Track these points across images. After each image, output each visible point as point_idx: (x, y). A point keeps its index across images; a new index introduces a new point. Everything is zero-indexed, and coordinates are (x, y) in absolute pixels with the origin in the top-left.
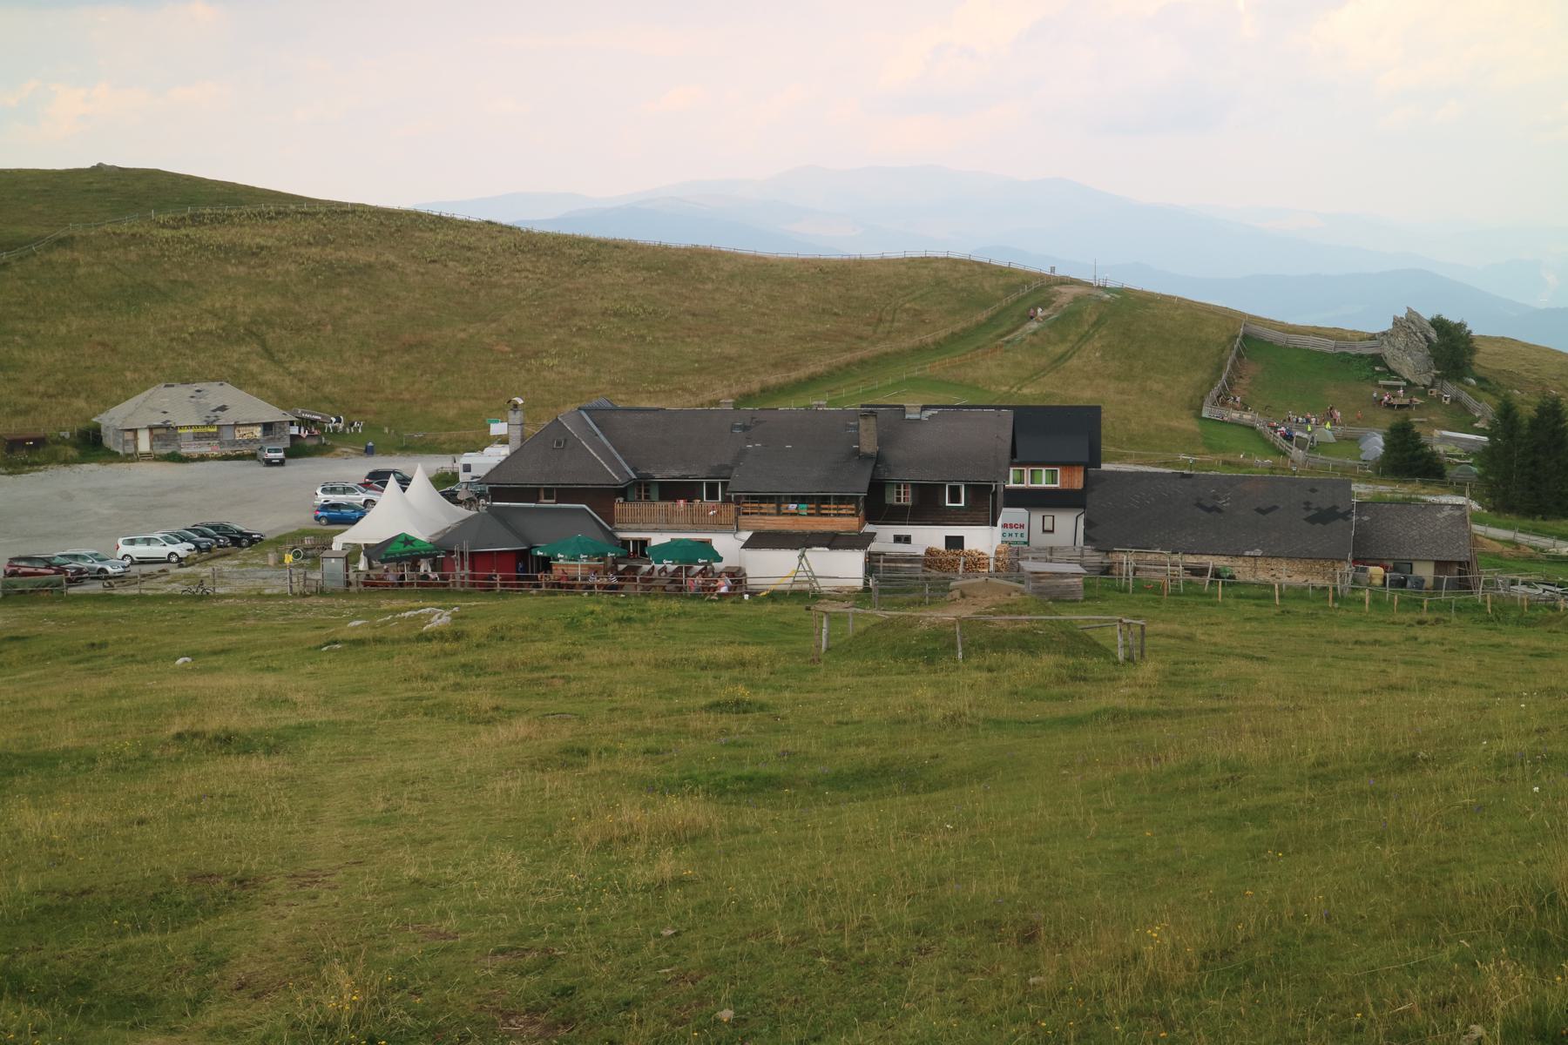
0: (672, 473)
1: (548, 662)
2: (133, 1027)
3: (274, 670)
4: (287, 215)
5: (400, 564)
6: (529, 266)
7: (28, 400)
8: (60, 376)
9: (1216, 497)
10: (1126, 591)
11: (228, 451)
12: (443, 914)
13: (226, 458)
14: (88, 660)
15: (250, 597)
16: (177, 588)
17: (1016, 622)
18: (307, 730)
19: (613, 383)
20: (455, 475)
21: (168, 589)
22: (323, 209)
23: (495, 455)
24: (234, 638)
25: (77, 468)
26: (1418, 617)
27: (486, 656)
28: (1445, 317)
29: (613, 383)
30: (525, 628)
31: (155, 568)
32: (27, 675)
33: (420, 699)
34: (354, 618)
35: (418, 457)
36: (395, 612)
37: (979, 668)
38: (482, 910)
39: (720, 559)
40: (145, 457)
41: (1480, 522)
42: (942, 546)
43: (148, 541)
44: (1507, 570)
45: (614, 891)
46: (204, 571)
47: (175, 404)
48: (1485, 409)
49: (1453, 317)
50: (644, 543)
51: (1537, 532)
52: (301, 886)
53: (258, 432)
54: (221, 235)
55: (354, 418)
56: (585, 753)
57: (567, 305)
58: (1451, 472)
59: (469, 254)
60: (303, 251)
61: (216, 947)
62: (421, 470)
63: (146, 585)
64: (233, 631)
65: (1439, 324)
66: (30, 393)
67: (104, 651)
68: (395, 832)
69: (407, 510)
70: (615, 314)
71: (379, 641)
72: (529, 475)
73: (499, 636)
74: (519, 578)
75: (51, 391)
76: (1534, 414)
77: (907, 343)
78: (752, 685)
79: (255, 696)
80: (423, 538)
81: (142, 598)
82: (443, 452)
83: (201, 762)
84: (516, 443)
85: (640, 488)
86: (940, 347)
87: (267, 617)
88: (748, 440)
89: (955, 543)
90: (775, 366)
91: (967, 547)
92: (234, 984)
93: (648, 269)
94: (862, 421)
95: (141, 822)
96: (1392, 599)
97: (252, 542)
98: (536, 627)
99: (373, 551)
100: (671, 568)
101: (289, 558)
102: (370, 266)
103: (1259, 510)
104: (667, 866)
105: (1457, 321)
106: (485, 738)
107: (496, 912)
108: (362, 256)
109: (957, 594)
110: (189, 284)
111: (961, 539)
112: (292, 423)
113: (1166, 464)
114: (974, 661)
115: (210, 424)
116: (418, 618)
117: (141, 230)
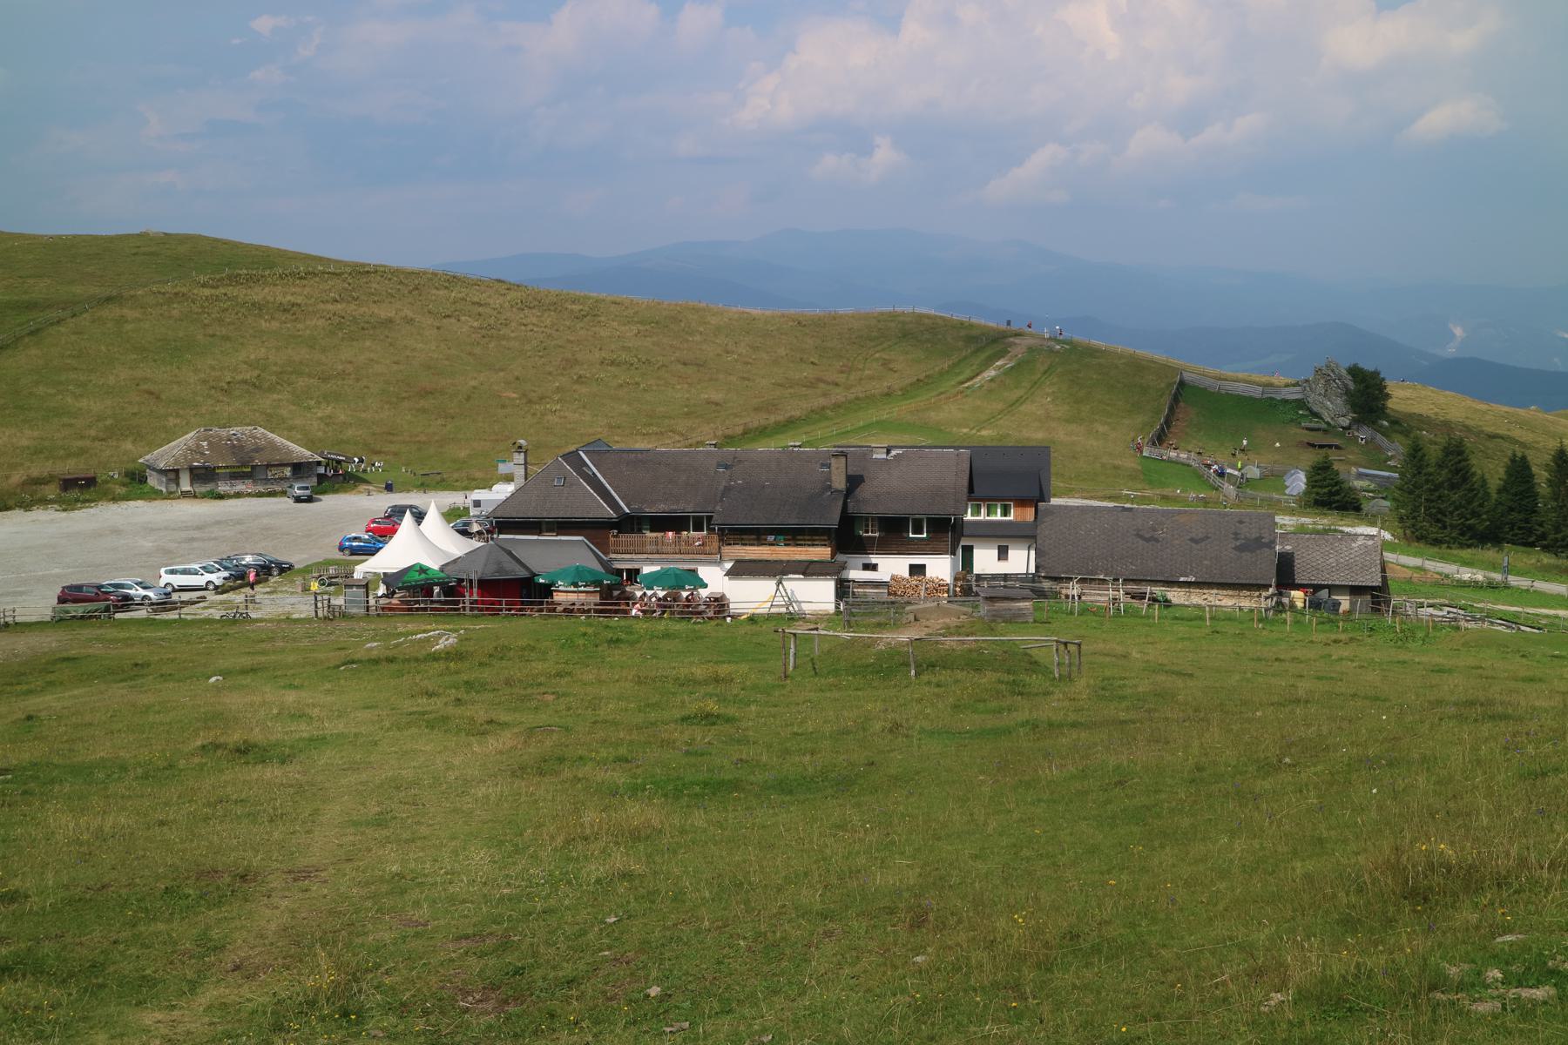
0: (660, 508)
1: (542, 679)
2: (139, 1004)
3: (296, 687)
4: (315, 275)
5: (420, 592)
6: (534, 320)
7: (80, 443)
8: (108, 422)
9: (1155, 530)
10: (1072, 613)
12: (417, 904)
13: (260, 495)
14: (131, 679)
15: (279, 621)
16: (216, 614)
17: (963, 642)
18: (318, 741)
19: (610, 427)
20: (467, 509)
21: (205, 614)
22: (348, 270)
23: (502, 491)
24: (263, 659)
25: (124, 505)
26: (1334, 637)
27: (486, 675)
28: (1361, 365)
29: (610, 427)
30: (523, 649)
31: (194, 595)
32: (76, 692)
33: (424, 713)
34: (373, 639)
35: (432, 493)
36: (407, 634)
37: (929, 683)
38: (452, 900)
39: (706, 586)
40: (185, 495)
41: (1393, 550)
42: (906, 574)
43: (185, 572)
44: (1416, 593)
45: (569, 883)
46: (237, 597)
48: (1396, 449)
49: (1368, 366)
50: (637, 571)
51: (1443, 559)
52: (295, 880)
53: (288, 472)
54: (258, 294)
55: (375, 458)
56: (561, 760)
57: (569, 355)
58: (1366, 507)
59: (481, 309)
60: (330, 307)
61: (215, 933)
62: (434, 504)
63: (185, 610)
64: (264, 653)
65: (1355, 372)
66: (82, 437)
67: (145, 671)
68: (385, 832)
69: (426, 543)
70: (613, 363)
71: (391, 660)
72: (530, 512)
73: (501, 653)
74: (522, 603)
75: (101, 435)
76: (1440, 454)
77: (877, 387)
78: (722, 699)
79: (275, 711)
80: (436, 567)
81: (181, 622)
82: (454, 489)
83: (221, 771)
84: (520, 481)
85: (629, 524)
87: (294, 640)
89: (917, 570)
90: (757, 409)
91: (929, 574)
92: (230, 966)
93: (641, 323)
94: (833, 461)
95: (162, 823)
96: (1310, 621)
97: (282, 571)
98: (533, 649)
99: (388, 579)
100: (661, 594)
101: (315, 586)
102: (391, 321)
103: (1192, 540)
104: (619, 860)
105: (1371, 369)
106: (476, 748)
107: (464, 901)
108: (384, 312)
109: (911, 617)
110: (227, 338)
111: (923, 566)
112: (319, 463)
113: (1110, 498)
114: (925, 678)
115: (244, 465)
116: (427, 640)
117: (184, 290)
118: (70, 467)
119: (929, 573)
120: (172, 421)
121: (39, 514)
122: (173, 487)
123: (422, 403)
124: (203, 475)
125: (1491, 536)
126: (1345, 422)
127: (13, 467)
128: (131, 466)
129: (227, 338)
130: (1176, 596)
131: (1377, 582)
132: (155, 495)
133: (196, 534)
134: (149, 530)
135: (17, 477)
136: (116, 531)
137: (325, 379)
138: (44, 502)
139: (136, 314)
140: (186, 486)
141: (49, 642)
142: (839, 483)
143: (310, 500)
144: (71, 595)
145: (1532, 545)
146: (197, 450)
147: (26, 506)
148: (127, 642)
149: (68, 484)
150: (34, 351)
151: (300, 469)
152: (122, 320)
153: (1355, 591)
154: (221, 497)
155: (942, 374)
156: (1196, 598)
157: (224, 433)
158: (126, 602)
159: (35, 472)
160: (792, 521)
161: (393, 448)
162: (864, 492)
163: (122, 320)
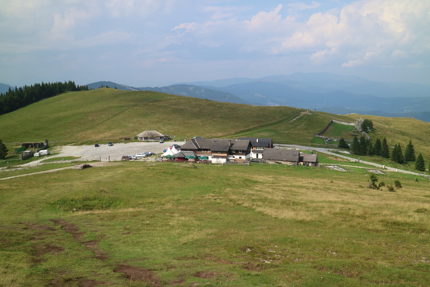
0: (205, 148)
5: (171, 159)
7: (128, 132)
40: (143, 141)
53: (159, 138)
69: (173, 152)
85: (200, 150)
86: (276, 123)
89: (240, 158)
118: (126, 136)
120: (143, 128)
121: (121, 144)
123: (185, 125)
124: (146, 138)
125: (372, 154)
126: (361, 130)
127: (118, 136)
129: (153, 113)
130: (283, 162)
131: (315, 161)
132: (139, 141)
134: (137, 147)
135: (118, 138)
136: (132, 147)
137: (169, 121)
138: (122, 142)
140: (143, 140)
141: (120, 164)
142: (229, 145)
143: (162, 143)
144: (124, 157)
146: (145, 134)
147: (119, 143)
148: (130, 164)
149: (126, 139)
150: (122, 115)
151: (161, 137)
152: (137, 109)
153: (312, 163)
154: (149, 142)
156: (285, 163)
157: (150, 131)
158: (131, 159)
159: (121, 137)
160: (221, 150)
161: (178, 134)
162: (233, 146)
163: (137, 109)
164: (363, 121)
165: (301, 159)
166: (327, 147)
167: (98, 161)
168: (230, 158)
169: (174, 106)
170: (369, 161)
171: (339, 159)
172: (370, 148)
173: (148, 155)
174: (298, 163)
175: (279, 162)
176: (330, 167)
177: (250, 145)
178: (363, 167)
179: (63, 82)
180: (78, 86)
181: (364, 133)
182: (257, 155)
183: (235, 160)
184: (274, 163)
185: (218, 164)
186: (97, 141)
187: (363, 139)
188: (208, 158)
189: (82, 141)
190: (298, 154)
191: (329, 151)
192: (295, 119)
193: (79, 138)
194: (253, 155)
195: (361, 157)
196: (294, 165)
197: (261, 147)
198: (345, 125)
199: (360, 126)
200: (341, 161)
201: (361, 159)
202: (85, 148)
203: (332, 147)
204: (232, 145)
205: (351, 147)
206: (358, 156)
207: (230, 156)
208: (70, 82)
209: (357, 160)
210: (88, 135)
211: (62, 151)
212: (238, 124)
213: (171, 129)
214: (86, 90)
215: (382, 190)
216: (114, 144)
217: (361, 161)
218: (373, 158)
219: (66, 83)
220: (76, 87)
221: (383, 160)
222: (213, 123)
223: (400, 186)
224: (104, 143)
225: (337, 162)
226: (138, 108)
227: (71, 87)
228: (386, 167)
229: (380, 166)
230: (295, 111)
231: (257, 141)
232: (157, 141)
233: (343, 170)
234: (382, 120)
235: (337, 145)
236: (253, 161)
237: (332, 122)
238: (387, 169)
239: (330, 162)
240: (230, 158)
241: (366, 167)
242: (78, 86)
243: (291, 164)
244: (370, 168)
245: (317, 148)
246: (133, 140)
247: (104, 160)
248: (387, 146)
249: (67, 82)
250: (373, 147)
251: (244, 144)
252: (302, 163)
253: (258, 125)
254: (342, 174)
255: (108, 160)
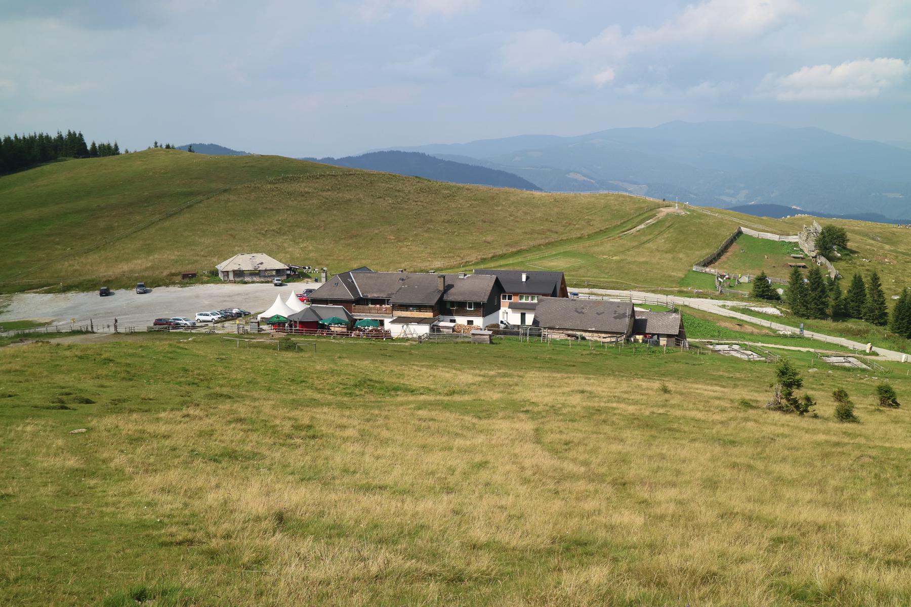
7: (195, 258)
11: (262, 280)
13: (262, 282)
40: (231, 282)
42: (466, 324)
47: (243, 261)
53: (274, 273)
85: (361, 301)
88: (404, 284)
89: (470, 322)
102: (350, 200)
110: (272, 209)
119: (475, 323)
121: (172, 289)
122: (226, 278)
123: (350, 241)
125: (841, 314)
126: (814, 254)
127: (166, 268)
128: (212, 269)
129: (272, 209)
130: (587, 335)
131: (677, 333)
132: (220, 282)
133: (228, 299)
134: (210, 296)
135: (166, 273)
136: (197, 297)
137: (309, 229)
138: (174, 284)
139: (235, 198)
140: (231, 277)
142: (441, 288)
143: (281, 285)
144: (158, 322)
145: (861, 318)
147: (167, 285)
149: (185, 276)
151: (279, 272)
152: (228, 200)
153: (669, 336)
154: (246, 283)
155: (615, 227)
156: (595, 337)
158: (177, 326)
159: (173, 271)
162: (452, 290)
164: (820, 229)
165: (638, 326)
166: (721, 296)
167: (87, 332)
168: (442, 324)
169: (330, 193)
170: (830, 332)
171: (749, 329)
172: (836, 299)
173: (227, 317)
174: (630, 336)
175: (579, 333)
176: (718, 347)
177: (499, 290)
178: (812, 350)
179: (54, 136)
180: (94, 144)
181: (822, 260)
182: (523, 315)
183: (453, 329)
184: (563, 337)
185: (408, 340)
186: (108, 282)
187: (816, 276)
188: (382, 323)
189: (69, 282)
190: (629, 312)
191: (724, 306)
192: (642, 226)
193: (63, 274)
194: (508, 316)
195: (810, 322)
196: (617, 342)
197: (533, 294)
198: (774, 241)
199: (813, 244)
200: (752, 334)
201: (809, 328)
202: (75, 298)
203: (735, 297)
204: (448, 288)
205: (784, 297)
206: (803, 320)
207: (441, 317)
208: (72, 136)
209: (797, 331)
210: (88, 267)
211: (9, 308)
212: (489, 238)
213: (311, 251)
214: (114, 154)
215: (816, 416)
216: (154, 290)
217: (807, 334)
218: (841, 325)
219: (60, 137)
220: (89, 148)
221: (867, 331)
222: (426, 235)
223: (894, 401)
224: (127, 287)
225: (743, 336)
226: (232, 197)
227: (73, 146)
228: (874, 349)
229: (859, 346)
230: (643, 205)
231: (524, 279)
232: (267, 282)
233: (755, 357)
234: (878, 230)
235: (746, 292)
236: (510, 331)
237: (740, 233)
238: (877, 355)
239: (722, 334)
240: (442, 324)
241: (821, 348)
242: (94, 144)
243: (608, 340)
244: (829, 352)
245: (692, 299)
246: (205, 279)
247: (103, 328)
248: (880, 294)
249: (65, 134)
250: (843, 297)
251: (484, 286)
252: (640, 338)
253: (543, 241)
254: (748, 366)
255: (112, 330)
